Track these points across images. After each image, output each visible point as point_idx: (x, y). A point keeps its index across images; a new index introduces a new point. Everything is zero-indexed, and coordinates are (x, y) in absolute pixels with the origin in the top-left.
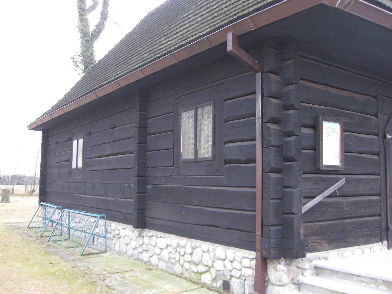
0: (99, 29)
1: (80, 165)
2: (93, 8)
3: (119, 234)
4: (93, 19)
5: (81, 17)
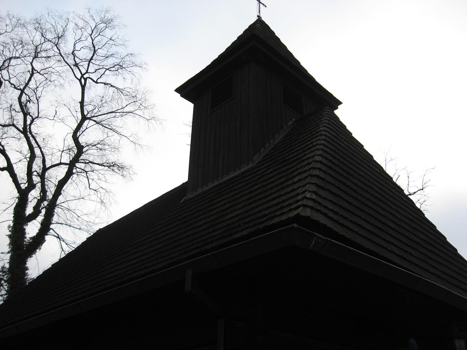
0: (39, 240)
2: (33, 216)
4: (32, 229)
5: (17, 225)
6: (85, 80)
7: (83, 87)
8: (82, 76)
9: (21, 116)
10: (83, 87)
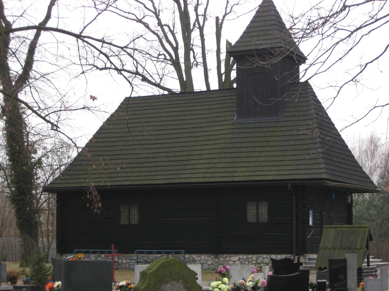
3: (194, 260)
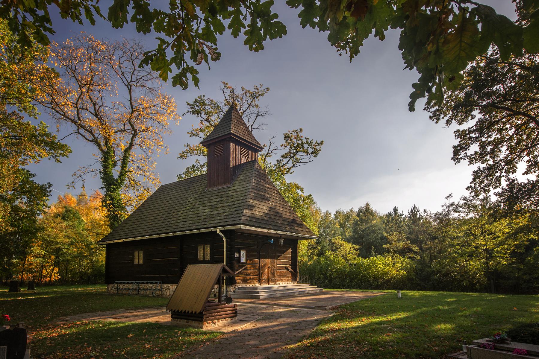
1: (141, 262)
6: (131, 86)
7: (130, 91)
8: (129, 83)
9: (92, 105)
10: (130, 91)
